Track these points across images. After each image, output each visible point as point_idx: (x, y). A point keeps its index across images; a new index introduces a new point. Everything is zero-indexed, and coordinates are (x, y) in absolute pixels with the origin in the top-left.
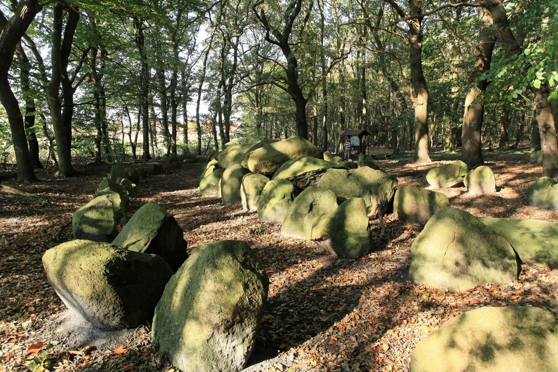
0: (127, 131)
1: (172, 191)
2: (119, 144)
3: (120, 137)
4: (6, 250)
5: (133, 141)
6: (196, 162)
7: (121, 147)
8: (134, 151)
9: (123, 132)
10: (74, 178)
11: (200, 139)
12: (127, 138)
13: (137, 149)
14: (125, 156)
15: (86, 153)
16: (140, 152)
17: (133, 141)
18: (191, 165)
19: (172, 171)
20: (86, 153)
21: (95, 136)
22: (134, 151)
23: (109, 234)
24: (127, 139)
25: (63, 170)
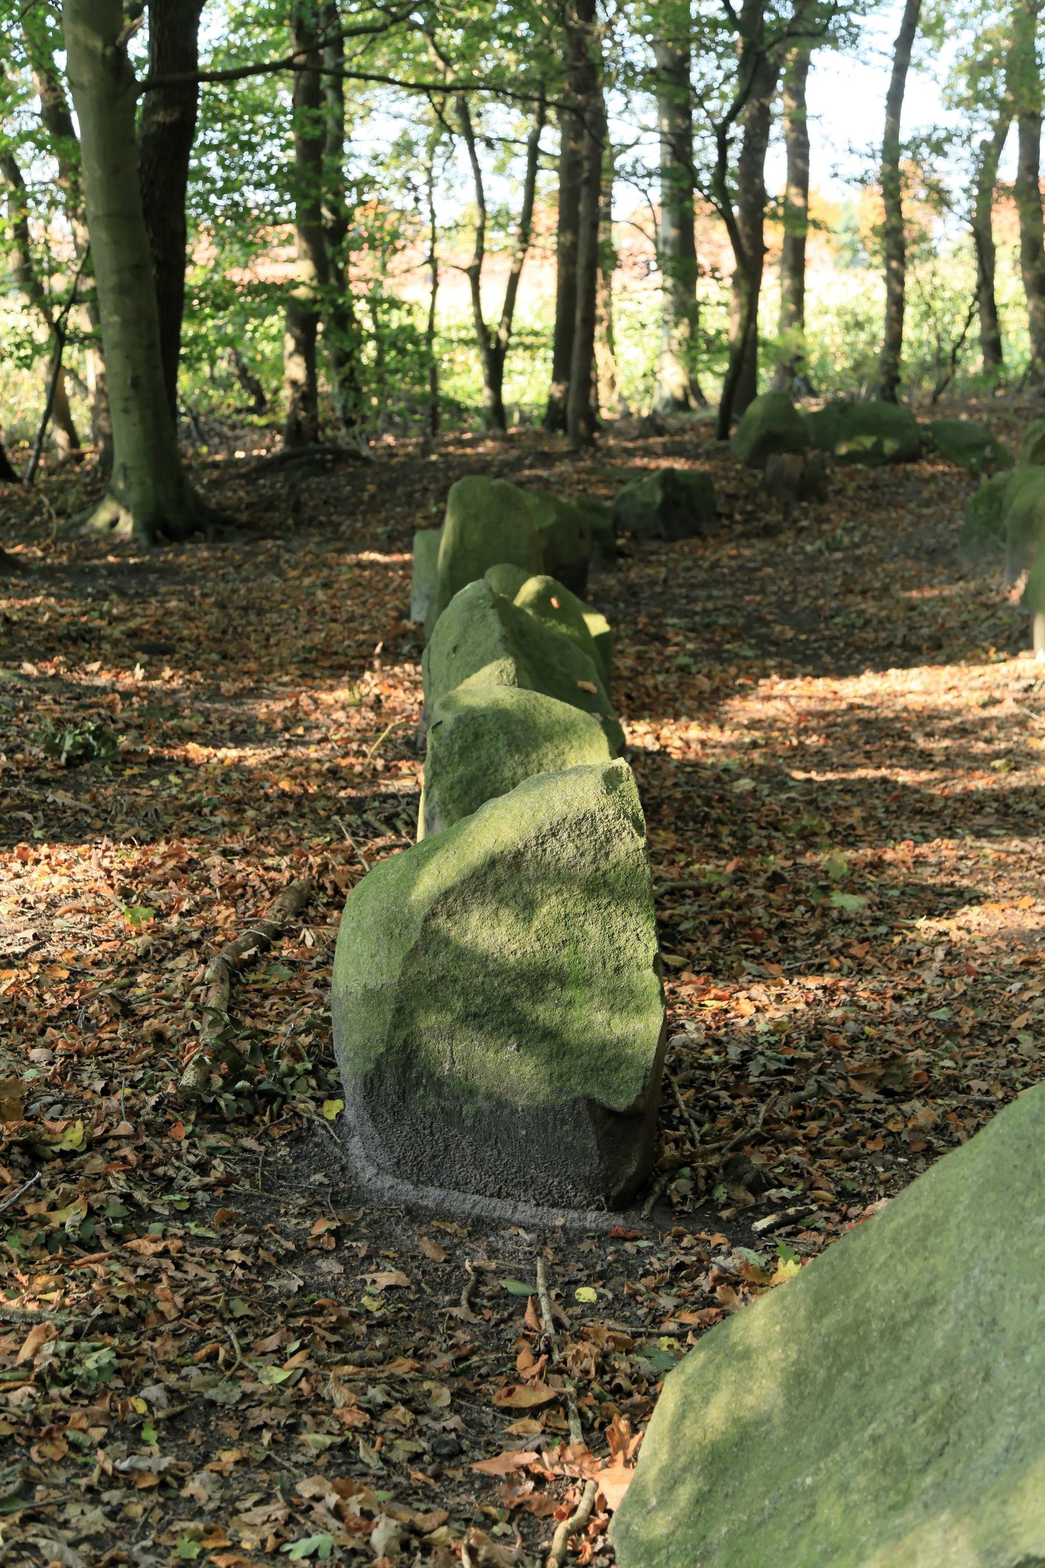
0: (459, 250)
1: (841, 673)
2: (408, 332)
3: (413, 290)
4: (451, 1456)
5: (492, 315)
6: (914, 457)
7: (415, 350)
8: (495, 378)
9: (432, 260)
10: (198, 554)
11: (897, 303)
12: (455, 290)
13: (514, 362)
14: (438, 410)
15: (223, 384)
16: (530, 383)
17: (492, 315)
18: (884, 474)
19: (773, 517)
20: (223, 384)
21: (294, 284)
22: (495, 378)
23: (621, 1103)
24: (454, 311)
25: (134, 496)
